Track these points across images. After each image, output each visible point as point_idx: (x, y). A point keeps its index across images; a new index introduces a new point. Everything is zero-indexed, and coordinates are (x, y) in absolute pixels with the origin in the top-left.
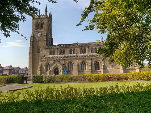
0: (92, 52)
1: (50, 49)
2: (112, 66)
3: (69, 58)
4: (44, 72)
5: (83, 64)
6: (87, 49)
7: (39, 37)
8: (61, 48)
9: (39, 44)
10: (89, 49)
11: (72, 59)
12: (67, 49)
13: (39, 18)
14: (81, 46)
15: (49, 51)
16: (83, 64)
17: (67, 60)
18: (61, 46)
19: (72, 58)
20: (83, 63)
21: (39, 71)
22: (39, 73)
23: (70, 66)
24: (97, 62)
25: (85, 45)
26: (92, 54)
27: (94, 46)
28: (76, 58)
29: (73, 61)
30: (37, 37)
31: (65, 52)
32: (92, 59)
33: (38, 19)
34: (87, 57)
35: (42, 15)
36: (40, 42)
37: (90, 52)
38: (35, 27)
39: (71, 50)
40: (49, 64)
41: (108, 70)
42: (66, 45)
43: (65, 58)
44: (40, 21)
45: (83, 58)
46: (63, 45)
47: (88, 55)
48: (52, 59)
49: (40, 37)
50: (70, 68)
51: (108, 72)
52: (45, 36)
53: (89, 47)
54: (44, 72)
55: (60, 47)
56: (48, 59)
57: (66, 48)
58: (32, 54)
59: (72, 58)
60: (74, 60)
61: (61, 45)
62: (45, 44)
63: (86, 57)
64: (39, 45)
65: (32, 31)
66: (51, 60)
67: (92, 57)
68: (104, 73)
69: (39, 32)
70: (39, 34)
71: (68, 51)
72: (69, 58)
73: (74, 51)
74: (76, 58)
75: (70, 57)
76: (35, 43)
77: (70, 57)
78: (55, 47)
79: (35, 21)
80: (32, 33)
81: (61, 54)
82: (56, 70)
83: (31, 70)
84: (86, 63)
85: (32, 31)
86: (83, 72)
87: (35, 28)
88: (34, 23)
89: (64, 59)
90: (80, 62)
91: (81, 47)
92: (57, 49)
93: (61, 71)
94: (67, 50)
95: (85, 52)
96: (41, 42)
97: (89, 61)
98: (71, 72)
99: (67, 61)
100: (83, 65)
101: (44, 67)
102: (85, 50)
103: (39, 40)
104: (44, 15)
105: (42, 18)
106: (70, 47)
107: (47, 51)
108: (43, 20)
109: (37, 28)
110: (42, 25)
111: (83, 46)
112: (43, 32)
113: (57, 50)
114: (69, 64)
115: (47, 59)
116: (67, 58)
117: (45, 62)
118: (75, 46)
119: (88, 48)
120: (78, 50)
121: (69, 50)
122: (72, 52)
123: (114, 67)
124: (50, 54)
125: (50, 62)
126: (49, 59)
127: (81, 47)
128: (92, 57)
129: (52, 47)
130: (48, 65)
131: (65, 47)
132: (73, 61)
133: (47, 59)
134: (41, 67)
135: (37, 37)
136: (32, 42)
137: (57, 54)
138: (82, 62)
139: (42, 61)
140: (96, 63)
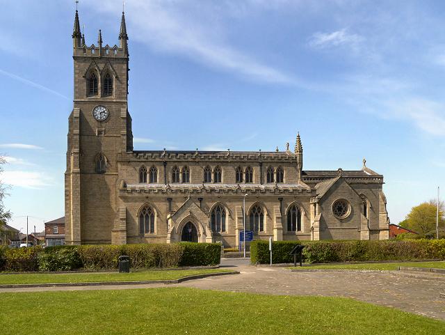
0: (174, 181)
1: (143, 164)
2: (341, 221)
3: (217, 195)
4: (137, 234)
5: (254, 215)
6: (256, 171)
7: (101, 122)
8: (176, 164)
9: (100, 144)
10: (263, 170)
11: (226, 198)
12: (198, 168)
13: (101, 58)
14: (238, 159)
15: (138, 168)
16: (254, 215)
17: (209, 202)
18: (153, 154)
19: (224, 195)
20: (256, 211)
21: (122, 231)
22: (123, 238)
23: (219, 219)
24: (294, 209)
25: (250, 159)
26: (175, 186)
27: (275, 164)
28: (237, 196)
29: (228, 204)
30: (93, 121)
31: (188, 174)
32: (281, 200)
33: (93, 58)
34: (268, 194)
35: (111, 46)
36: (105, 141)
37: (170, 179)
38: (84, 86)
39: (207, 170)
40: (150, 209)
41: (331, 231)
42: (193, 153)
43: (203, 195)
44: (102, 66)
45: (256, 195)
46: (185, 153)
47: (164, 187)
48: (160, 195)
49: (106, 120)
50: (219, 224)
51: (331, 237)
52: (122, 120)
53: (261, 164)
54: (137, 234)
55: (175, 159)
56: (147, 195)
57: (192, 163)
58: (79, 175)
59: (224, 195)
60: (230, 202)
61: (177, 153)
62: (125, 146)
63: (265, 193)
64: (102, 148)
65: (76, 97)
66: (159, 200)
67: (282, 195)
68: (321, 238)
69: (101, 104)
70: (100, 112)
71: (199, 173)
72: (217, 195)
73: (218, 173)
74: (237, 196)
75: (219, 193)
76: (86, 139)
77: (219, 193)
78: (158, 159)
79: (85, 66)
80: (75, 107)
81: (178, 181)
82: (190, 230)
83: (79, 229)
84: (155, 211)
85: (73, 98)
86: (257, 235)
87: (85, 88)
88: (81, 71)
89: (200, 196)
90: (247, 207)
91: (238, 165)
92: (165, 164)
93: (204, 233)
94: (196, 171)
95: (153, 180)
96: (107, 139)
97: (275, 206)
98: (220, 235)
99: (210, 204)
100: (257, 216)
101: (137, 221)
102: (176, 172)
103: (100, 133)
104: (115, 48)
105: (109, 59)
106: (207, 160)
107: (130, 169)
108: (114, 66)
109: (92, 89)
110: (111, 82)
111: (246, 160)
112: (114, 106)
113: (163, 168)
114: (213, 211)
115: (145, 195)
116: (210, 195)
117: (139, 205)
118: (222, 160)
119: (259, 167)
120: (228, 173)
121: (203, 170)
122: (210, 177)
123: (345, 225)
124: (142, 179)
125: (155, 203)
126: (152, 195)
127: (238, 165)
128: (282, 195)
129: (147, 159)
130: (147, 212)
131: (190, 159)
132: (228, 204)
133: (145, 195)
134: (128, 219)
135: (92, 123)
136: (78, 137)
137: (163, 180)
138: (144, 209)
139: (128, 202)
140: (291, 211)
